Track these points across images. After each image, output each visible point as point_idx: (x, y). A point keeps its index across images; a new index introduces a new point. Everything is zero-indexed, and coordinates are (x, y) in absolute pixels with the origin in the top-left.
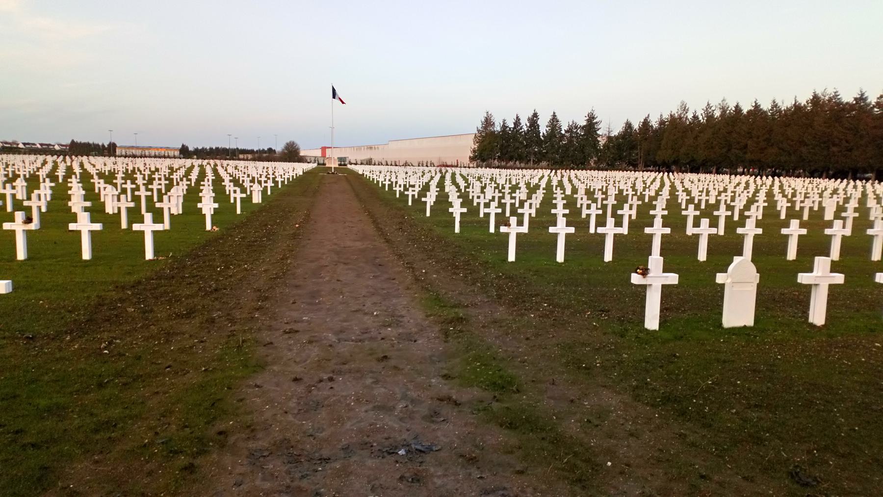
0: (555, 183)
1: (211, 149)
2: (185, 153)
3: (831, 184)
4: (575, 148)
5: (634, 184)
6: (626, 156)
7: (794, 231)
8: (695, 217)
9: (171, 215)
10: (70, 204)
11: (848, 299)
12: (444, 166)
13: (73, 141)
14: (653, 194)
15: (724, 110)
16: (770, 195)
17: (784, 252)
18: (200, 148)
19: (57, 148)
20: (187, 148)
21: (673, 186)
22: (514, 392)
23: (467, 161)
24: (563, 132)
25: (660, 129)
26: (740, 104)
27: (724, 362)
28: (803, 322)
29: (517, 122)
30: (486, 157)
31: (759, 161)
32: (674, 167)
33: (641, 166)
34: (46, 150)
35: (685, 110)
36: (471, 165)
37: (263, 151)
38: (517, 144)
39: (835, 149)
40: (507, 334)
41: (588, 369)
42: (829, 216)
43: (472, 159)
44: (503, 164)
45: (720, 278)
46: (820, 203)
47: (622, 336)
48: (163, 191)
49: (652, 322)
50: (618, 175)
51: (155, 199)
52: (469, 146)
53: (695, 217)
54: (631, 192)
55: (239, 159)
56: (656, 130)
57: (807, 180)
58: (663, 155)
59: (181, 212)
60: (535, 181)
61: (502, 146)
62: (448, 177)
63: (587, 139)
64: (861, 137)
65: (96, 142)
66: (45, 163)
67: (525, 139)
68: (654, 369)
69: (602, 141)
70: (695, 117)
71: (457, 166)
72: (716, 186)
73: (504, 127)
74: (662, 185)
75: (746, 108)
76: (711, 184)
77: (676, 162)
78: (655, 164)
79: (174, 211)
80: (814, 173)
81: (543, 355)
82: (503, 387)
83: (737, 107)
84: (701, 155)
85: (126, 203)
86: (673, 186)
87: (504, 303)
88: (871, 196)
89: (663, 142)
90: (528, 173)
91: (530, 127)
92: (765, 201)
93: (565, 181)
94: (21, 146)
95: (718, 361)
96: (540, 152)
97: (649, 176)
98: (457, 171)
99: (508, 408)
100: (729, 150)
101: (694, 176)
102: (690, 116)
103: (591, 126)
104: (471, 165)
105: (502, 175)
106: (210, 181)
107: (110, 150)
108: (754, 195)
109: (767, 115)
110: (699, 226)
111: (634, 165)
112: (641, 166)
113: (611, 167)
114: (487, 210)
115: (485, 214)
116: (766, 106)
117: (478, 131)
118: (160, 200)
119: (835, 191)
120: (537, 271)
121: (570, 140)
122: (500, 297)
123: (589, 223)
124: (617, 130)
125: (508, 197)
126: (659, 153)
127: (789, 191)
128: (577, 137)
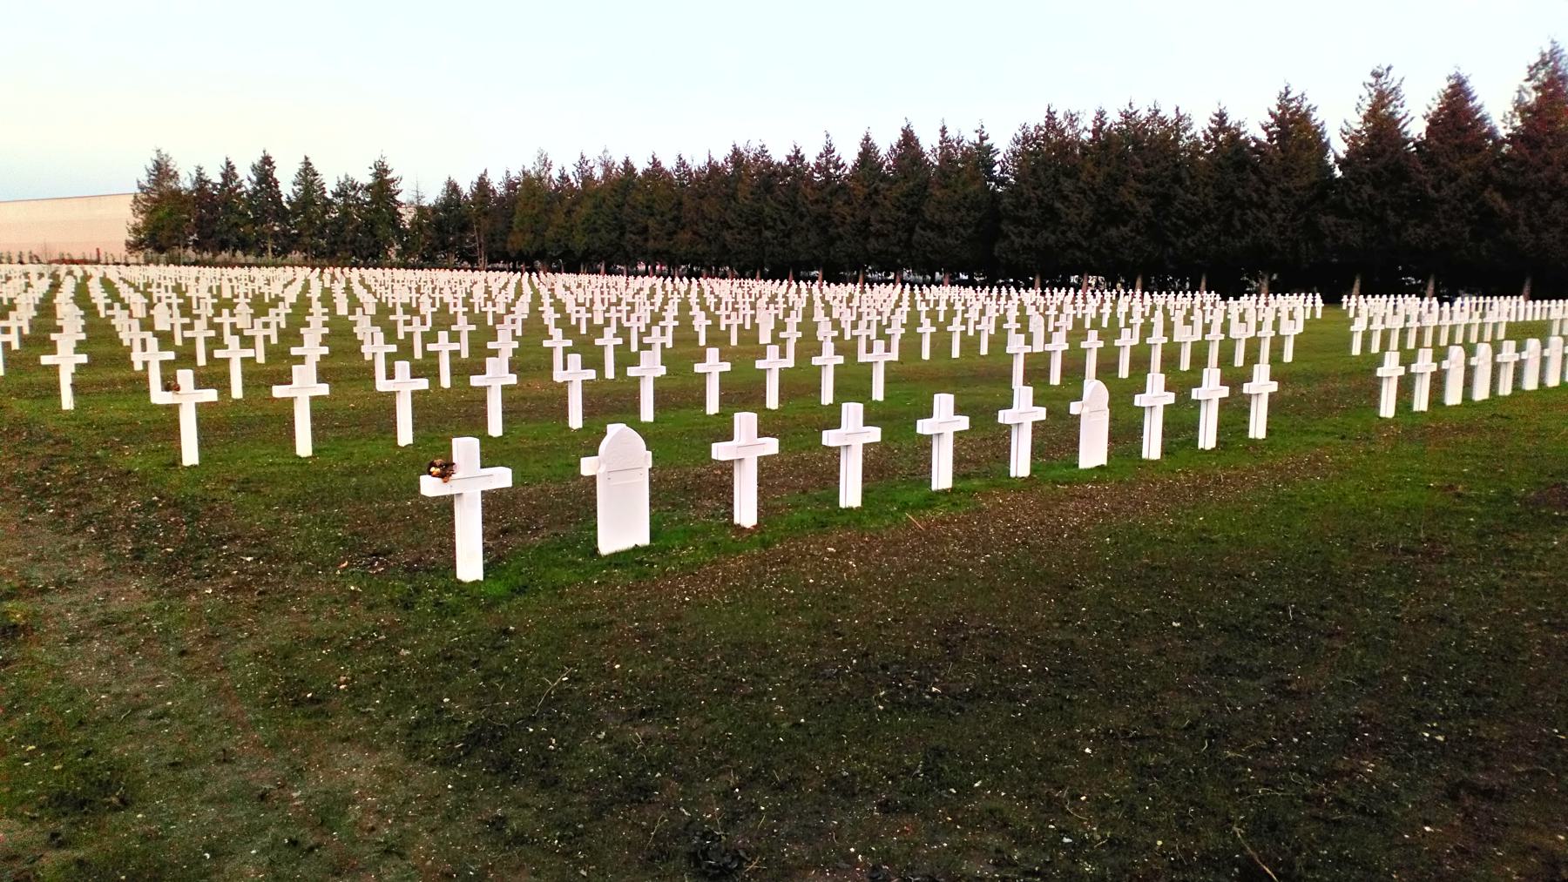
0: (315, 293)
3: (768, 287)
4: (358, 228)
5: (470, 295)
6: (453, 244)
7: (713, 366)
8: (164, 365)
11: (791, 473)
12: (63, 261)
15: (608, 167)
16: (684, 307)
17: (702, 403)
21: (536, 297)
22: (116, 809)
23: (121, 252)
24: (329, 195)
25: (508, 195)
26: (631, 160)
27: (596, 626)
28: (726, 525)
29: (229, 173)
30: (164, 243)
31: (667, 252)
32: (538, 264)
33: (482, 260)
35: (547, 165)
36: (132, 260)
38: (234, 218)
39: (768, 234)
40: (132, 651)
41: (319, 701)
42: (765, 337)
43: (133, 247)
44: (207, 256)
45: (587, 466)
46: (753, 317)
47: (406, 607)
49: (470, 565)
50: (442, 276)
52: (118, 221)
53: (164, 365)
54: (461, 309)
56: (501, 200)
57: (736, 282)
58: (518, 241)
60: (276, 289)
61: (196, 220)
62: (68, 287)
63: (377, 211)
64: (802, 217)
67: (250, 206)
68: (462, 673)
69: (408, 216)
70: (564, 178)
71: (98, 262)
72: (606, 296)
73: (201, 181)
74: (519, 292)
75: (641, 166)
76: (597, 291)
77: (541, 255)
78: (507, 259)
80: (747, 269)
81: (214, 690)
82: (82, 804)
83: (627, 162)
84: (579, 242)
86: (536, 297)
87: (146, 570)
88: (818, 304)
89: (516, 220)
90: (260, 274)
91: (259, 183)
92: (675, 318)
93: (338, 289)
95: (585, 626)
96: (285, 233)
97: (500, 280)
98: (96, 272)
99: (80, 863)
100: (622, 234)
101: (570, 279)
102: (555, 174)
103: (382, 186)
104: (132, 260)
105: (201, 280)
108: (662, 309)
109: (671, 179)
111: (469, 260)
112: (482, 260)
113: (429, 261)
114: (408, 329)
116: (669, 164)
117: (142, 188)
119: (773, 299)
120: (247, 481)
121: (345, 213)
122: (138, 554)
123: (147, 380)
124: (432, 195)
126: (512, 238)
127: (711, 301)
128: (359, 206)
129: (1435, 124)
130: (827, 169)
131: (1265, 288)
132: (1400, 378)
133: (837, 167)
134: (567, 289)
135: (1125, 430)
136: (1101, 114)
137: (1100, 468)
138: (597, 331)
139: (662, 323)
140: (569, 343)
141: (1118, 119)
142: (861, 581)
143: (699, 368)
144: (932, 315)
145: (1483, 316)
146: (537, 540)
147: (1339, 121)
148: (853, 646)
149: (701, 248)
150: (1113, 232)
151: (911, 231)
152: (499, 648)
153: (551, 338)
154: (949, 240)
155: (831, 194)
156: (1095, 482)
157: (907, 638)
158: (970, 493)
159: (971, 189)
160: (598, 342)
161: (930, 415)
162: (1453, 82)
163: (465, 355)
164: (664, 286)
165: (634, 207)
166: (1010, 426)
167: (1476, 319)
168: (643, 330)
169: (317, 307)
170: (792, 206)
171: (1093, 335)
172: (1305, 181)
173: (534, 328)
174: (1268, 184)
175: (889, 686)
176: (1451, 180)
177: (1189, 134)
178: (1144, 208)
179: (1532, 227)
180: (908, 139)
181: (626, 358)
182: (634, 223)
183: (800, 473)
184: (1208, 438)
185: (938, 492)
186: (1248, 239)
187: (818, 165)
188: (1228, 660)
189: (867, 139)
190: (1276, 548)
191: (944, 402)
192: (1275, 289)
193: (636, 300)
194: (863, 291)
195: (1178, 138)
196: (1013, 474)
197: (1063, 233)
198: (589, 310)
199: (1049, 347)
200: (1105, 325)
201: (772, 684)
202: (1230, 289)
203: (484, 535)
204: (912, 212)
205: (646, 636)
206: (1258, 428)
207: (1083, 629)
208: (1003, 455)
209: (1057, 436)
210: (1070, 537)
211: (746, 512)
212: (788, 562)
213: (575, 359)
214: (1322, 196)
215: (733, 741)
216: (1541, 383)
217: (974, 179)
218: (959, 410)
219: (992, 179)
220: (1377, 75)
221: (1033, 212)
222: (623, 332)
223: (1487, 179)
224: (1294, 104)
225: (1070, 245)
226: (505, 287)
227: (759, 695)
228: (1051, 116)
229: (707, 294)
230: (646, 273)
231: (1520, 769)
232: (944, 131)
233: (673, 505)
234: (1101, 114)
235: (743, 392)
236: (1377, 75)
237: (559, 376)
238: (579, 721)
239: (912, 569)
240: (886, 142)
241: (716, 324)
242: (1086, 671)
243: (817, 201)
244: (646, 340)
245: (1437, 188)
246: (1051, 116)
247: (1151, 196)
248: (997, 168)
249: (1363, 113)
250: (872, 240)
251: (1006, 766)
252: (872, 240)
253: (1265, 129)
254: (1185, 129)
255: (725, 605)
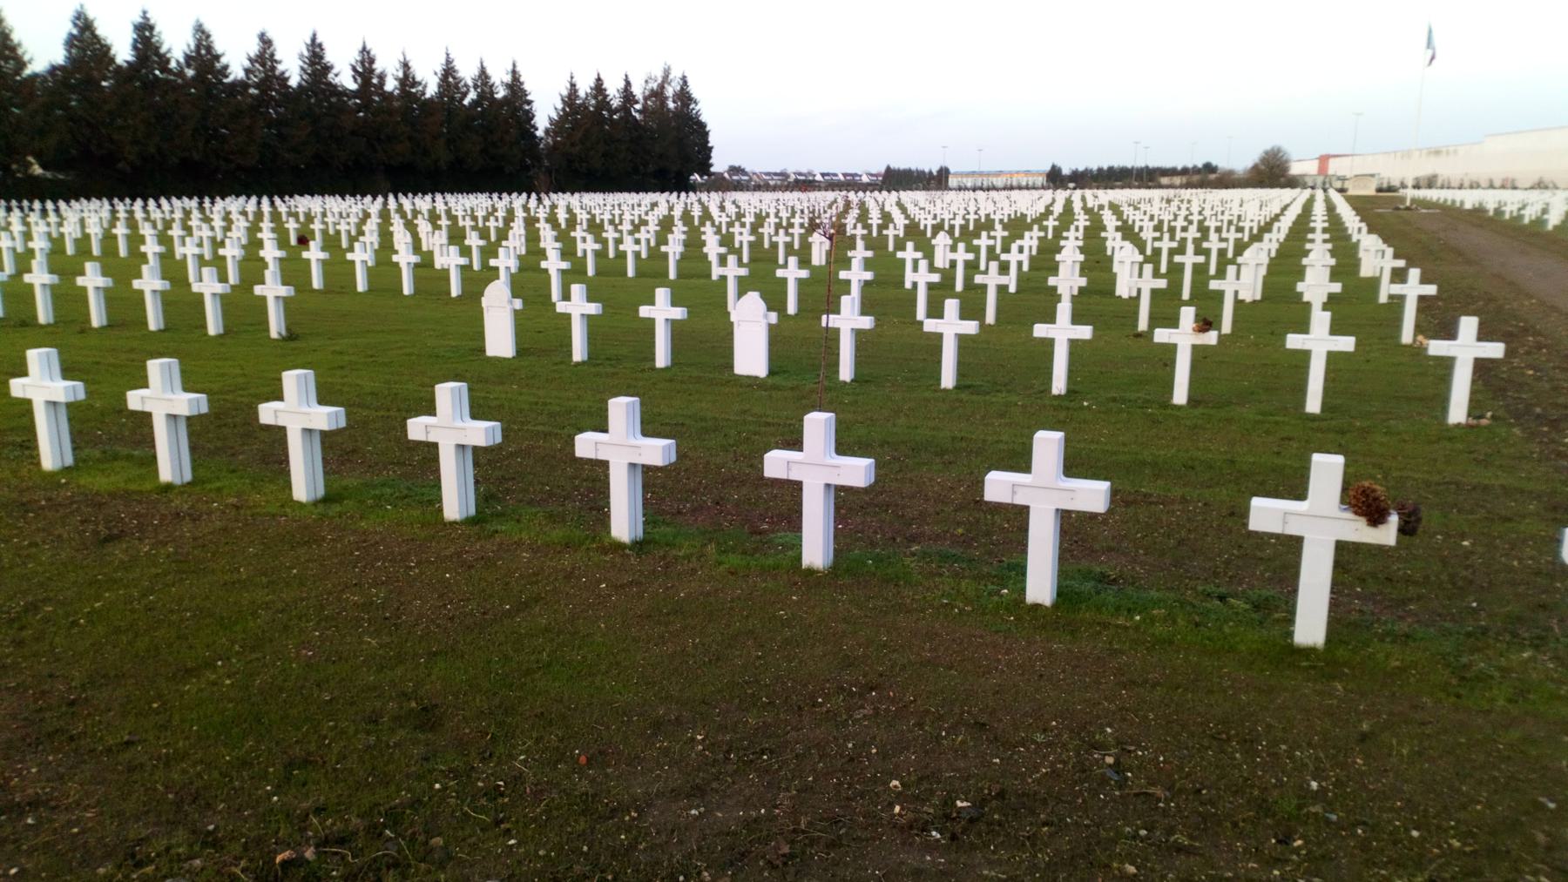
1: (1100, 170)
2: (1055, 178)
4: (805, 184)
9: (1238, 303)
10: (1300, 287)
13: (888, 169)
14: (501, 224)
15: (365, 68)
18: (1081, 169)
19: (865, 179)
20: (1060, 170)
34: (851, 183)
37: (1196, 170)
48: (1230, 255)
51: (1212, 271)
55: (1161, 187)
59: (1258, 297)
65: (920, 168)
66: (654, 205)
79: (1246, 296)
85: (1150, 283)
94: (819, 178)
106: (1081, 229)
107: (937, 180)
108: (1058, 233)
110: (941, 316)
115: (1391, 297)
118: (1221, 274)
125: (628, 240)
144: (552, 220)
163: (1012, 289)
169: (678, 223)
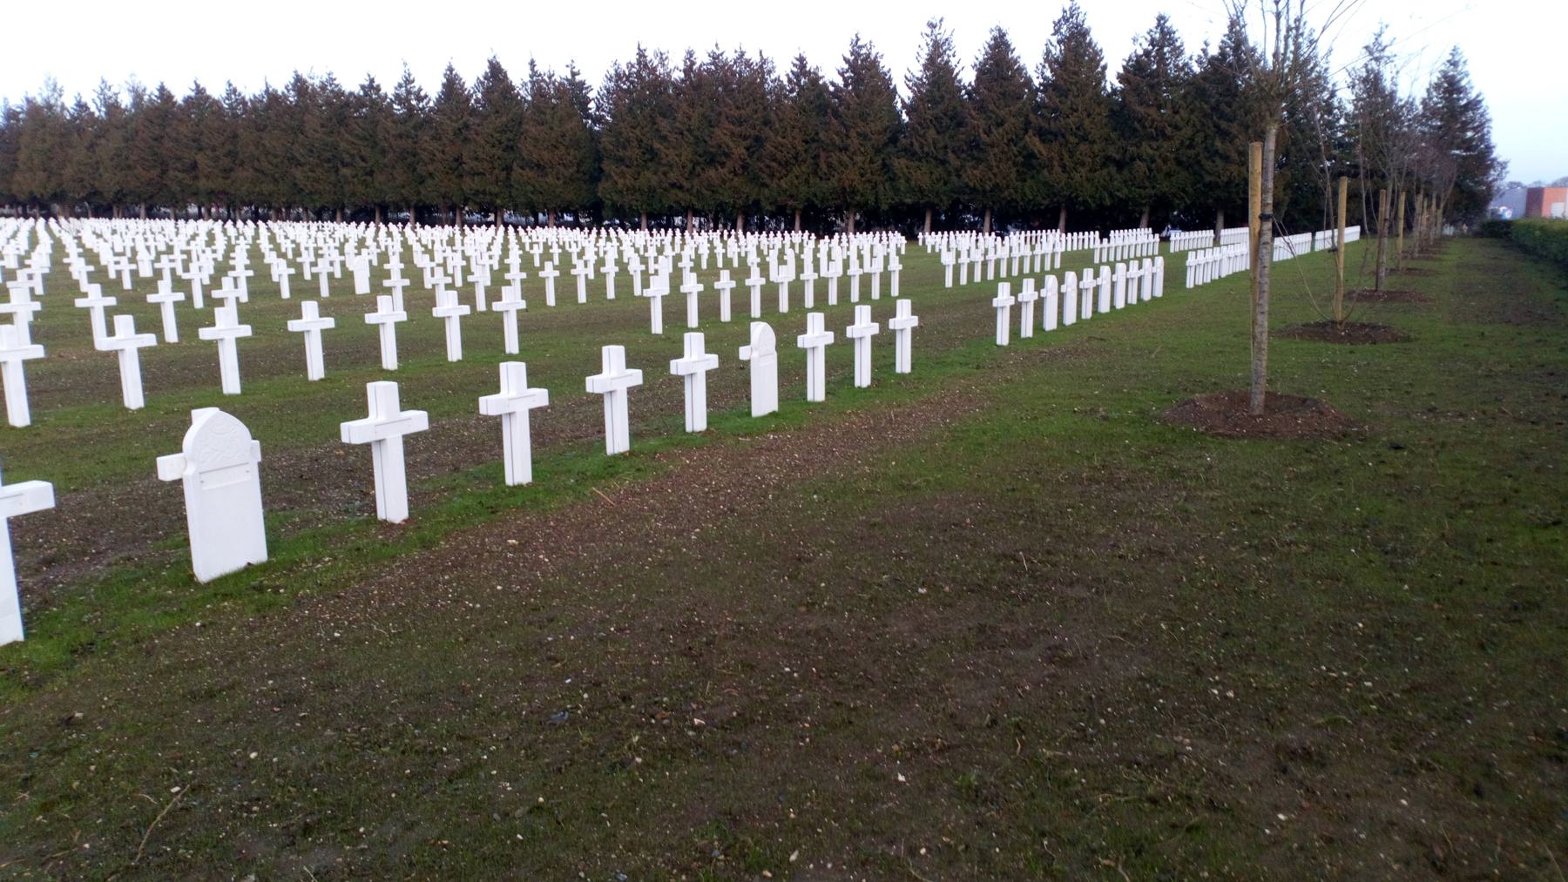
3: (353, 231)
7: (311, 323)
15: (138, 96)
17: (302, 366)
21: (58, 248)
26: (168, 86)
27: (211, 694)
32: (56, 207)
39: (346, 171)
45: (168, 468)
46: (343, 264)
57: (314, 226)
58: (26, 182)
64: (383, 152)
74: (33, 241)
75: (180, 93)
76: (139, 238)
77: (59, 197)
83: (162, 89)
84: (109, 182)
86: (58, 248)
88: (417, 248)
89: (22, 156)
100: (164, 172)
101: (101, 224)
102: (70, 103)
108: (227, 256)
109: (221, 108)
126: (18, 177)
127: (287, 246)
129: (982, 72)
130: (409, 101)
131: (851, 226)
132: (1012, 308)
133: (420, 99)
134: (99, 236)
135: (792, 370)
136: (690, 54)
137: (773, 414)
138: (151, 284)
139: (231, 273)
140: (112, 301)
141: (707, 60)
142: (563, 581)
143: (294, 326)
145: (1033, 248)
146: (99, 570)
147: (903, 69)
148: (578, 675)
149: (267, 187)
150: (711, 173)
151: (508, 169)
152: (62, 753)
153: (85, 295)
154: (550, 179)
155: (415, 128)
156: (774, 431)
157: (641, 652)
158: (652, 455)
159: (569, 126)
160: (151, 298)
161: (598, 370)
162: (996, 33)
164: (224, 231)
165: (176, 140)
166: (682, 377)
167: (1028, 253)
168: (207, 282)
170: (371, 140)
171: (725, 274)
172: (878, 126)
173: (59, 285)
174: (847, 128)
175: (640, 726)
176: (1000, 124)
177: (773, 76)
178: (739, 151)
179: (1064, 167)
180: (496, 72)
181: (192, 320)
182: (179, 159)
183: (455, 449)
184: (863, 376)
185: (615, 457)
186: (834, 181)
187: (397, 96)
188: (994, 629)
189: (451, 69)
190: (976, 490)
191: (613, 356)
192: (860, 228)
193: (193, 247)
194: (463, 233)
195: (764, 81)
196: (689, 429)
197: (665, 174)
198: (133, 260)
199: (647, 293)
200: (704, 266)
201: (485, 749)
202: (820, 223)
203: (17, 571)
204: (509, 149)
205: (290, 701)
206: (904, 363)
207: (832, 610)
208: (679, 408)
209: (730, 384)
210: (776, 498)
211: (392, 502)
212: (463, 565)
213: (125, 323)
214: (894, 140)
215: (453, 852)
216: (1112, 307)
217: (570, 116)
218: (630, 364)
219: (589, 116)
220: (932, 26)
221: (633, 152)
222: (180, 284)
223: (1027, 124)
224: (864, 51)
225: (673, 185)
226: (14, 236)
227: (468, 771)
228: (641, 54)
229: (280, 240)
230: (199, 217)
231: (1320, 721)
232: (532, 64)
233: (289, 501)
234: (690, 54)
235: (353, 352)
236: (932, 26)
237: (102, 342)
238: (210, 860)
239: (618, 558)
240: (472, 76)
241: (300, 274)
242: (855, 665)
243: (400, 136)
244: (216, 294)
245: (988, 132)
246: (641, 54)
247: (745, 138)
248: (592, 105)
249: (923, 61)
250: (467, 179)
251: (820, 823)
252: (467, 179)
253: (842, 74)
254: (770, 72)
255: (392, 636)
